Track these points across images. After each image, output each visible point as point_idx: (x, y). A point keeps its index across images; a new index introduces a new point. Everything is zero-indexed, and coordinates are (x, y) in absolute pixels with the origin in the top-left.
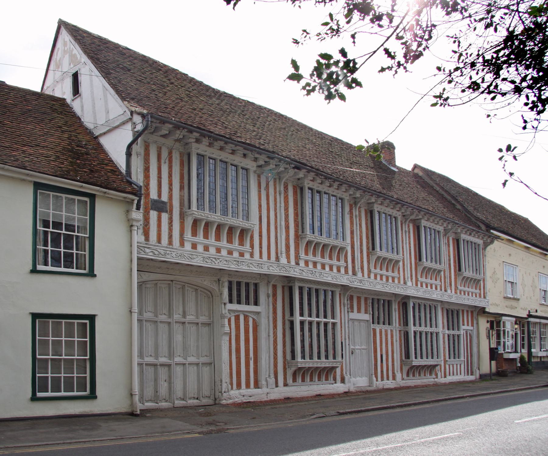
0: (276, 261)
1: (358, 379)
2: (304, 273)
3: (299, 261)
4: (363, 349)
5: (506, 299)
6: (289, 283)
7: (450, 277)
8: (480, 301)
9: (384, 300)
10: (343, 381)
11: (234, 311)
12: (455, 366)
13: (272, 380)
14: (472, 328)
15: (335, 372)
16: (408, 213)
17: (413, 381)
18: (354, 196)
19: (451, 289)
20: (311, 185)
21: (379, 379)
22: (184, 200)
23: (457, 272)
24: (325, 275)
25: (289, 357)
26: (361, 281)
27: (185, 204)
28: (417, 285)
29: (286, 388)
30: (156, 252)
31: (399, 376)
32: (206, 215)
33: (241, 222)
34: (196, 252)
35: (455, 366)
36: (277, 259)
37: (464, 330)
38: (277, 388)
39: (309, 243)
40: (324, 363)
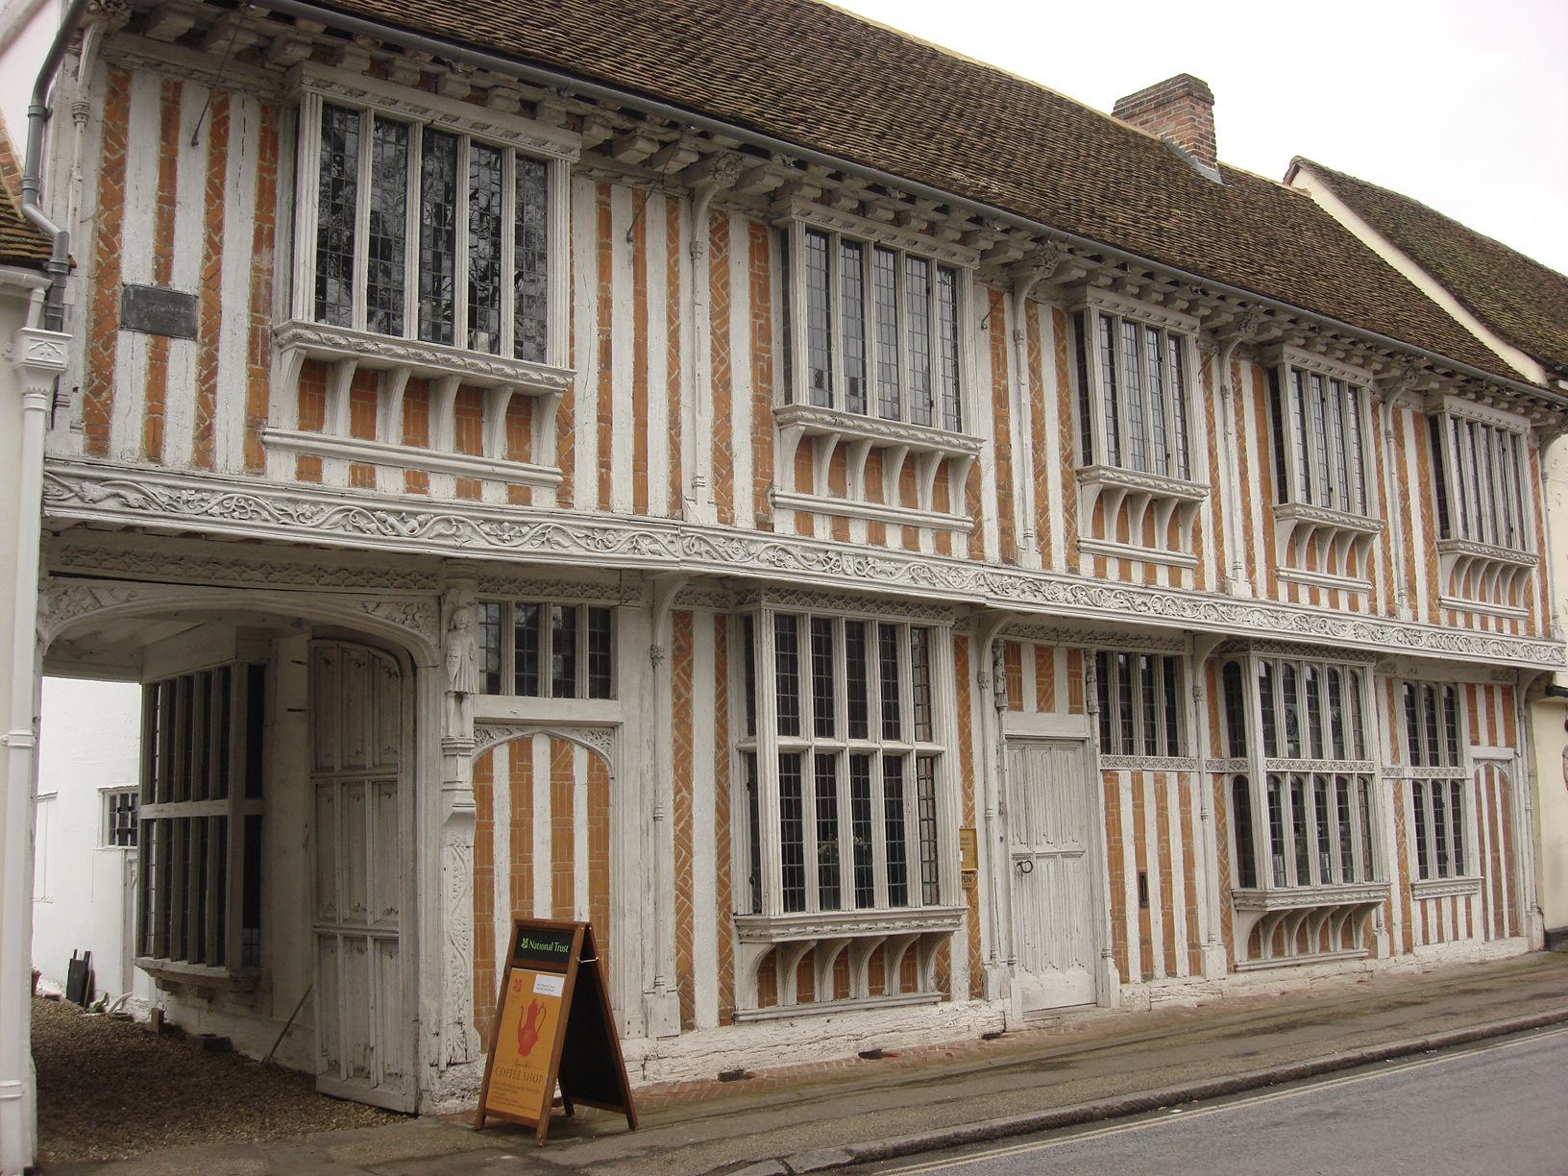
1: (1050, 975)
2: (791, 562)
3: (769, 514)
7: (1410, 561)
9: (1150, 659)
11: (505, 724)
12: (1446, 904)
13: (668, 1006)
14: (1508, 753)
16: (1226, 318)
17: (1278, 973)
18: (1002, 259)
20: (818, 216)
21: (1135, 973)
22: (269, 285)
24: (879, 565)
25: (741, 903)
26: (1036, 587)
28: (1273, 593)
29: (734, 1035)
30: (132, 497)
31: (1215, 958)
37: (1477, 760)
38: (691, 1034)
40: (883, 919)
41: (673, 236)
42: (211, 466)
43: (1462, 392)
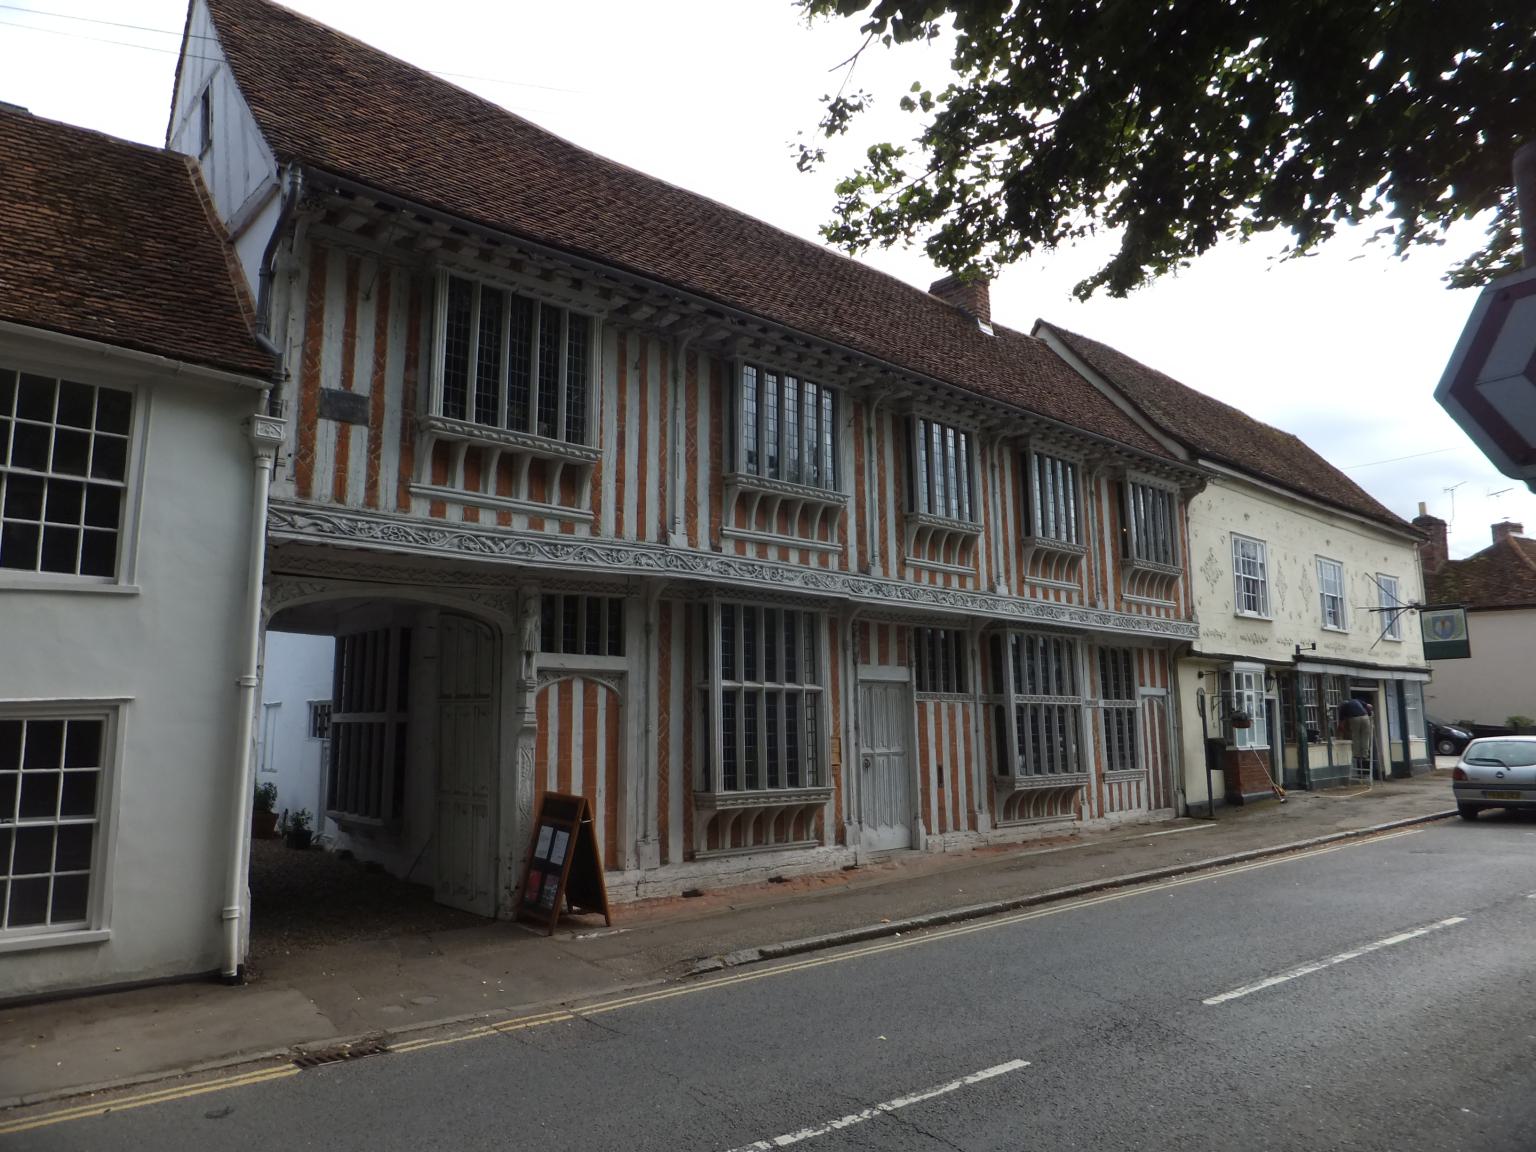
0: (659, 542)
2: (732, 571)
4: (895, 754)
5: (1240, 622)
6: (700, 597)
8: (1178, 628)
10: (841, 839)
11: (556, 672)
12: (1125, 787)
13: (651, 850)
15: (821, 817)
19: (1106, 601)
21: (935, 829)
22: (415, 392)
23: (1121, 558)
24: (786, 574)
26: (878, 588)
27: (413, 400)
28: (1021, 592)
29: (693, 868)
30: (326, 526)
32: (470, 428)
33: (564, 446)
34: (439, 524)
35: (1125, 787)
36: (664, 537)
37: (1144, 696)
39: (1038, 553)
40: (784, 795)
41: (663, 366)
42: (376, 507)
43: (1137, 467)
